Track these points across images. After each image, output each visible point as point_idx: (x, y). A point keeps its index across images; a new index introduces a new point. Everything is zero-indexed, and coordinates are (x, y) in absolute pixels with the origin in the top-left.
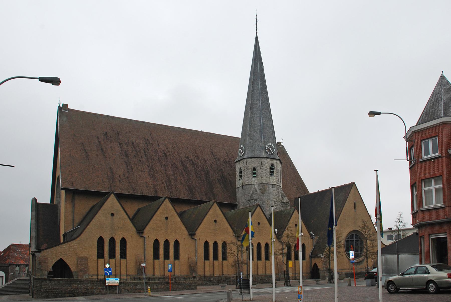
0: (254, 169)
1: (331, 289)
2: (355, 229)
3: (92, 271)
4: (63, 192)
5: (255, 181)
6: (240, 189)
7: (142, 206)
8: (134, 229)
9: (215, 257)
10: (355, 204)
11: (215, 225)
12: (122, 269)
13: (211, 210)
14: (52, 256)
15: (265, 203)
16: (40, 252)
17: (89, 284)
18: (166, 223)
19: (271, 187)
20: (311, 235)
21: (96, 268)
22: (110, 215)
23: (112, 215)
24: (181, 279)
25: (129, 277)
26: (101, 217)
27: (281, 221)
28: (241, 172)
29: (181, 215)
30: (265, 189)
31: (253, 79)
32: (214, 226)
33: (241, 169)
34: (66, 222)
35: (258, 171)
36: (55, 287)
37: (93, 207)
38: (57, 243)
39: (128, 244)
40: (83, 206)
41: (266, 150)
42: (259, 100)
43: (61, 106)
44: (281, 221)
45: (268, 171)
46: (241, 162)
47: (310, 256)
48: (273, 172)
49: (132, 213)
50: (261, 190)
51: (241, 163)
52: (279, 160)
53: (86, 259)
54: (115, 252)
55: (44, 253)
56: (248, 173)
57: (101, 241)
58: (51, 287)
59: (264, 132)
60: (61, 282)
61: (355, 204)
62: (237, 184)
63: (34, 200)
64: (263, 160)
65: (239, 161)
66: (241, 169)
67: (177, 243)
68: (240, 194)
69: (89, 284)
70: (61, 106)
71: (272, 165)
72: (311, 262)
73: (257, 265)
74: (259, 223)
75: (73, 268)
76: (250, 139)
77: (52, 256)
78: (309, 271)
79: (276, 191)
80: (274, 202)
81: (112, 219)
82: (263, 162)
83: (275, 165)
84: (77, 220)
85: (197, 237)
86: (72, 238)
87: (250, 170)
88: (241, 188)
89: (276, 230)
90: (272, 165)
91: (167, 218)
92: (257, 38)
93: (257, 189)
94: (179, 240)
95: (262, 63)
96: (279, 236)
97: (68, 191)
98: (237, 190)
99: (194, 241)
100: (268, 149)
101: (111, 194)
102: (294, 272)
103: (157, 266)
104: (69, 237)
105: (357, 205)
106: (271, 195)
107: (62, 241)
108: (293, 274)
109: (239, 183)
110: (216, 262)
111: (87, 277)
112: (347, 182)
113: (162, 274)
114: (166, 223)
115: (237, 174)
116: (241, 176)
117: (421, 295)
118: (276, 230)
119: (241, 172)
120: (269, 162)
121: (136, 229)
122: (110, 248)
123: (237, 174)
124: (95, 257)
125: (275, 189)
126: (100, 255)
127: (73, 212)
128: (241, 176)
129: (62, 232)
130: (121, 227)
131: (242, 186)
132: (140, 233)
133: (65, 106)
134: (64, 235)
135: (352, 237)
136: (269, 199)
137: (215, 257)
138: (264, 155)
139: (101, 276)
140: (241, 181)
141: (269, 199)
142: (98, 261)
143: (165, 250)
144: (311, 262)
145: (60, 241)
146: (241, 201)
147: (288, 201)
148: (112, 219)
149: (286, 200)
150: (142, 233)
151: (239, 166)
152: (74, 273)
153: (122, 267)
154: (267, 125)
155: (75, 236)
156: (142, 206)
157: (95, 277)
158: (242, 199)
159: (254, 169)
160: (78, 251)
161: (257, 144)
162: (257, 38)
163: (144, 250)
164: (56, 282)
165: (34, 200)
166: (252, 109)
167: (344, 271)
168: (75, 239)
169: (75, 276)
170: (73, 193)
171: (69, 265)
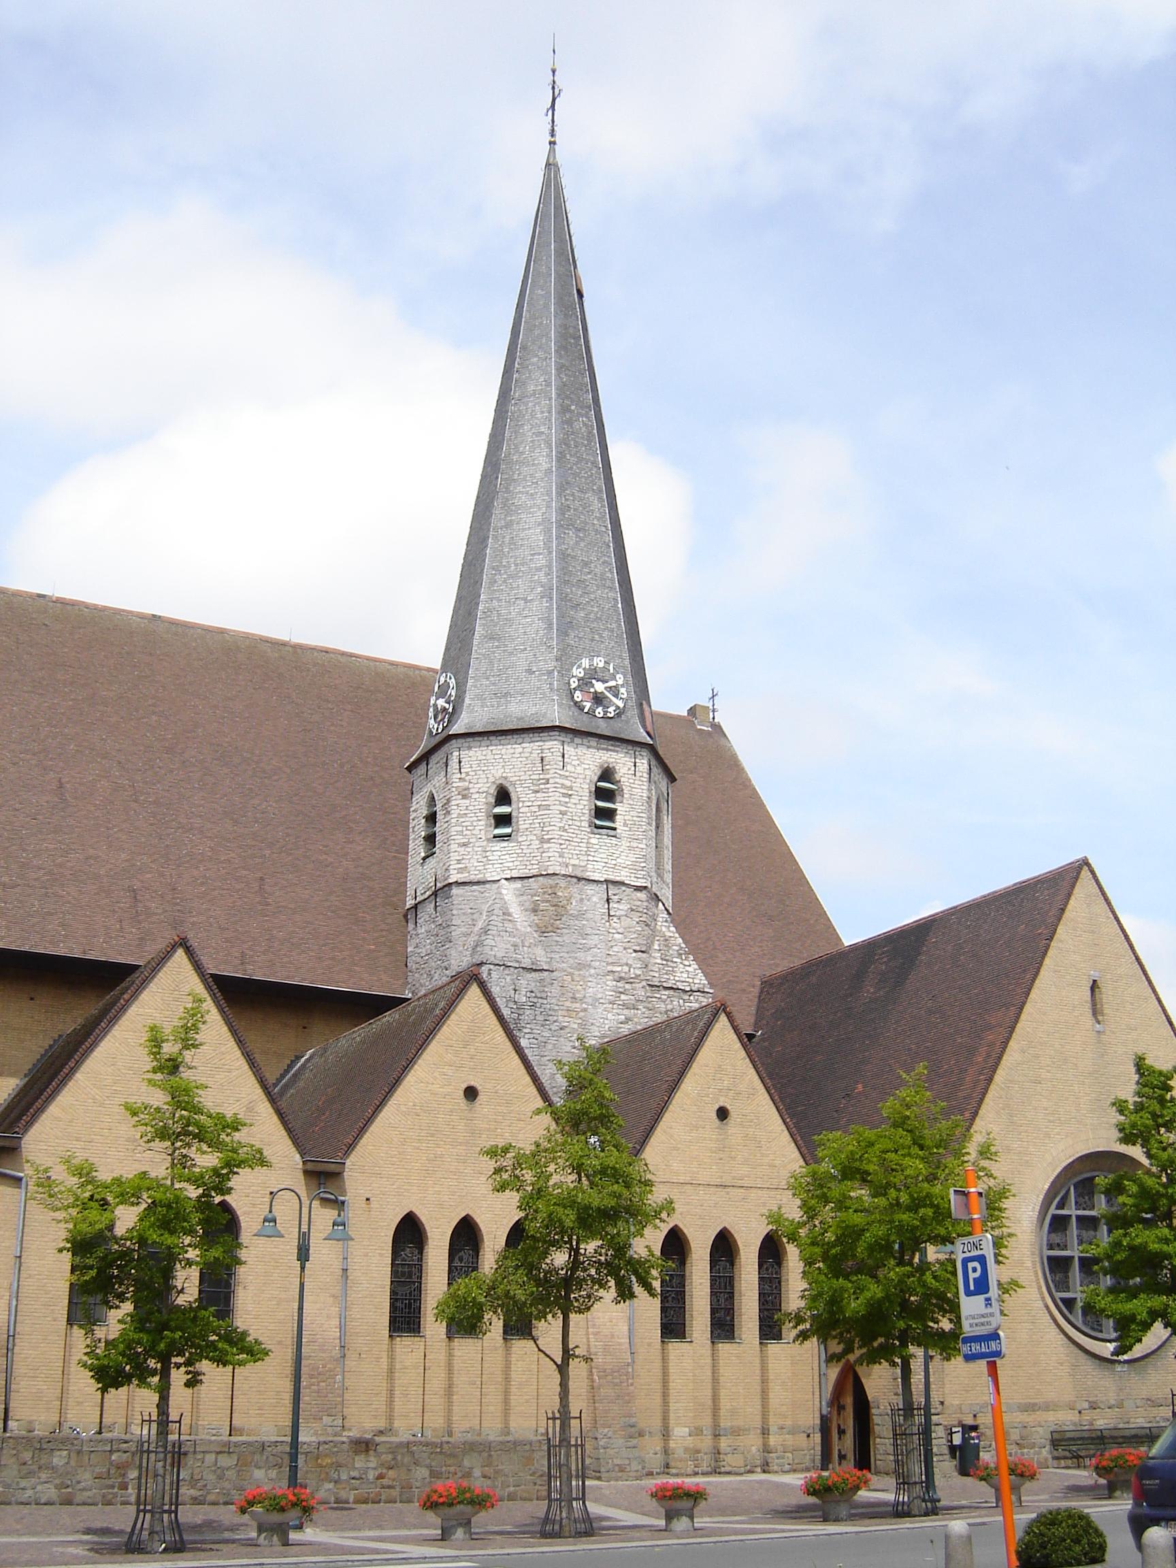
0: (503, 796)
5: (502, 860)
10: (1094, 986)
15: (555, 990)
19: (596, 895)
28: (431, 819)
30: (560, 909)
33: (432, 799)
35: (523, 807)
45: (583, 804)
46: (434, 759)
48: (609, 814)
52: (652, 749)
56: (467, 819)
64: (552, 746)
66: (432, 799)
71: (607, 774)
73: (715, 1380)
74: (471, 1093)
79: (626, 922)
90: (607, 774)
93: (515, 910)
102: (707, 1421)
103: (407, 1380)
105: (1107, 994)
106: (593, 941)
108: (697, 1432)
115: (418, 828)
116: (431, 839)
117: (105, 1032)
119: (431, 819)
120: (586, 762)
125: (620, 908)
128: (431, 839)
131: (435, 894)
135: (1086, 1189)
141: (582, 966)
147: (700, 980)
154: (586, 564)
159: (503, 796)
161: (522, 661)
162: (551, 166)
167: (1041, 1416)
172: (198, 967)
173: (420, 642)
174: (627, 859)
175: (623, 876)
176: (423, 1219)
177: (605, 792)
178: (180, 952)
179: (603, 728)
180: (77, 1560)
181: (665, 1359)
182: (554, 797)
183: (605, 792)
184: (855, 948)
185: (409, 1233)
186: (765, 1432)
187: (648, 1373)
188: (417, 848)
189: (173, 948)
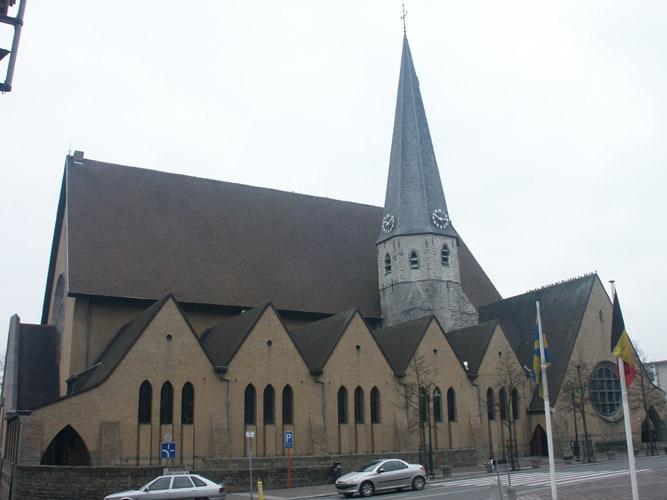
0: (414, 254)
1: (619, 479)
2: (604, 359)
3: (128, 450)
4: (70, 302)
6: (388, 292)
7: (219, 323)
8: (209, 365)
9: (359, 418)
10: (600, 312)
11: (358, 354)
12: (184, 445)
13: (349, 327)
14: (50, 421)
16: (28, 414)
17: (130, 478)
18: (268, 355)
19: (444, 285)
20: (525, 370)
21: (134, 445)
22: (165, 339)
23: (169, 337)
24: (295, 463)
25: (198, 461)
26: (149, 344)
27: (467, 347)
28: (388, 261)
29: (203, 340)
30: (435, 290)
31: (404, 105)
32: (357, 359)
33: (388, 255)
34: (74, 358)
35: (421, 256)
36: (58, 485)
37: (124, 329)
38: (55, 398)
39: (296, 396)
40: (107, 325)
41: (432, 221)
42: (416, 137)
43: (72, 154)
44: (467, 347)
45: (439, 257)
46: (388, 242)
47: (527, 412)
48: (445, 260)
49: (200, 333)
50: (427, 290)
51: (389, 245)
53: (115, 425)
54: (171, 411)
55: (38, 415)
56: (401, 266)
57: (146, 388)
58: (50, 484)
59: (427, 190)
60: (72, 474)
61: (600, 312)
62: (380, 283)
63: (16, 319)
64: (429, 237)
65: (385, 241)
66: (388, 255)
67: (188, 390)
68: (387, 300)
69: (130, 478)
70: (72, 154)
71: (445, 247)
72: (529, 422)
75: (91, 445)
76: (404, 202)
77: (50, 421)
78: (528, 442)
80: (455, 310)
81: (167, 349)
82: (429, 242)
83: (450, 246)
84: (95, 354)
85: (325, 379)
86: (83, 388)
87: (407, 257)
88: (390, 289)
89: (466, 364)
91: (270, 343)
92: (405, 40)
93: (421, 291)
94: (379, 388)
95: (416, 79)
96: (472, 375)
97: (78, 297)
98: (381, 293)
99: (321, 386)
100: (437, 219)
101: (164, 301)
104: (78, 385)
107: (63, 391)
109: (384, 280)
110: (361, 428)
111: (118, 462)
112: (588, 271)
113: (261, 452)
114: (268, 355)
116: (388, 268)
118: (466, 364)
119: (388, 261)
120: (439, 242)
121: (213, 364)
122: (165, 404)
123: (382, 265)
124: (135, 421)
125: (451, 289)
126: (144, 416)
127: (88, 339)
128: (388, 268)
129: (65, 374)
130: (185, 362)
131: (392, 285)
132: (220, 372)
133: (79, 154)
134: (70, 383)
136: (442, 308)
137: (359, 418)
138: (430, 229)
139: (144, 459)
140: (389, 276)
141: (442, 308)
142: (139, 429)
143: (267, 405)
144: (529, 422)
145: (59, 393)
146: (389, 312)
147: (474, 311)
148: (167, 349)
149: (471, 308)
150: (225, 371)
151: (382, 252)
152: (92, 456)
153: (185, 441)
155: (92, 381)
156: (219, 323)
157: (133, 462)
158: (392, 311)
159: (414, 254)
160: (104, 414)
162: (405, 40)
163: (228, 406)
164: (45, 473)
165: (16, 319)
166: (403, 152)
168: (96, 386)
169: (94, 461)
170: (91, 303)
171: (83, 437)
172: (174, 300)
173: (376, 197)
174: (453, 274)
175: (452, 279)
176: (294, 390)
177: (445, 253)
178: (170, 299)
179: (443, 233)
180: (413, 485)
181: (182, 428)
182: (430, 255)
183: (445, 253)
184: (506, 300)
185: (342, 391)
186: (138, 459)
187: (332, 432)
188: (382, 270)
189: (167, 298)
